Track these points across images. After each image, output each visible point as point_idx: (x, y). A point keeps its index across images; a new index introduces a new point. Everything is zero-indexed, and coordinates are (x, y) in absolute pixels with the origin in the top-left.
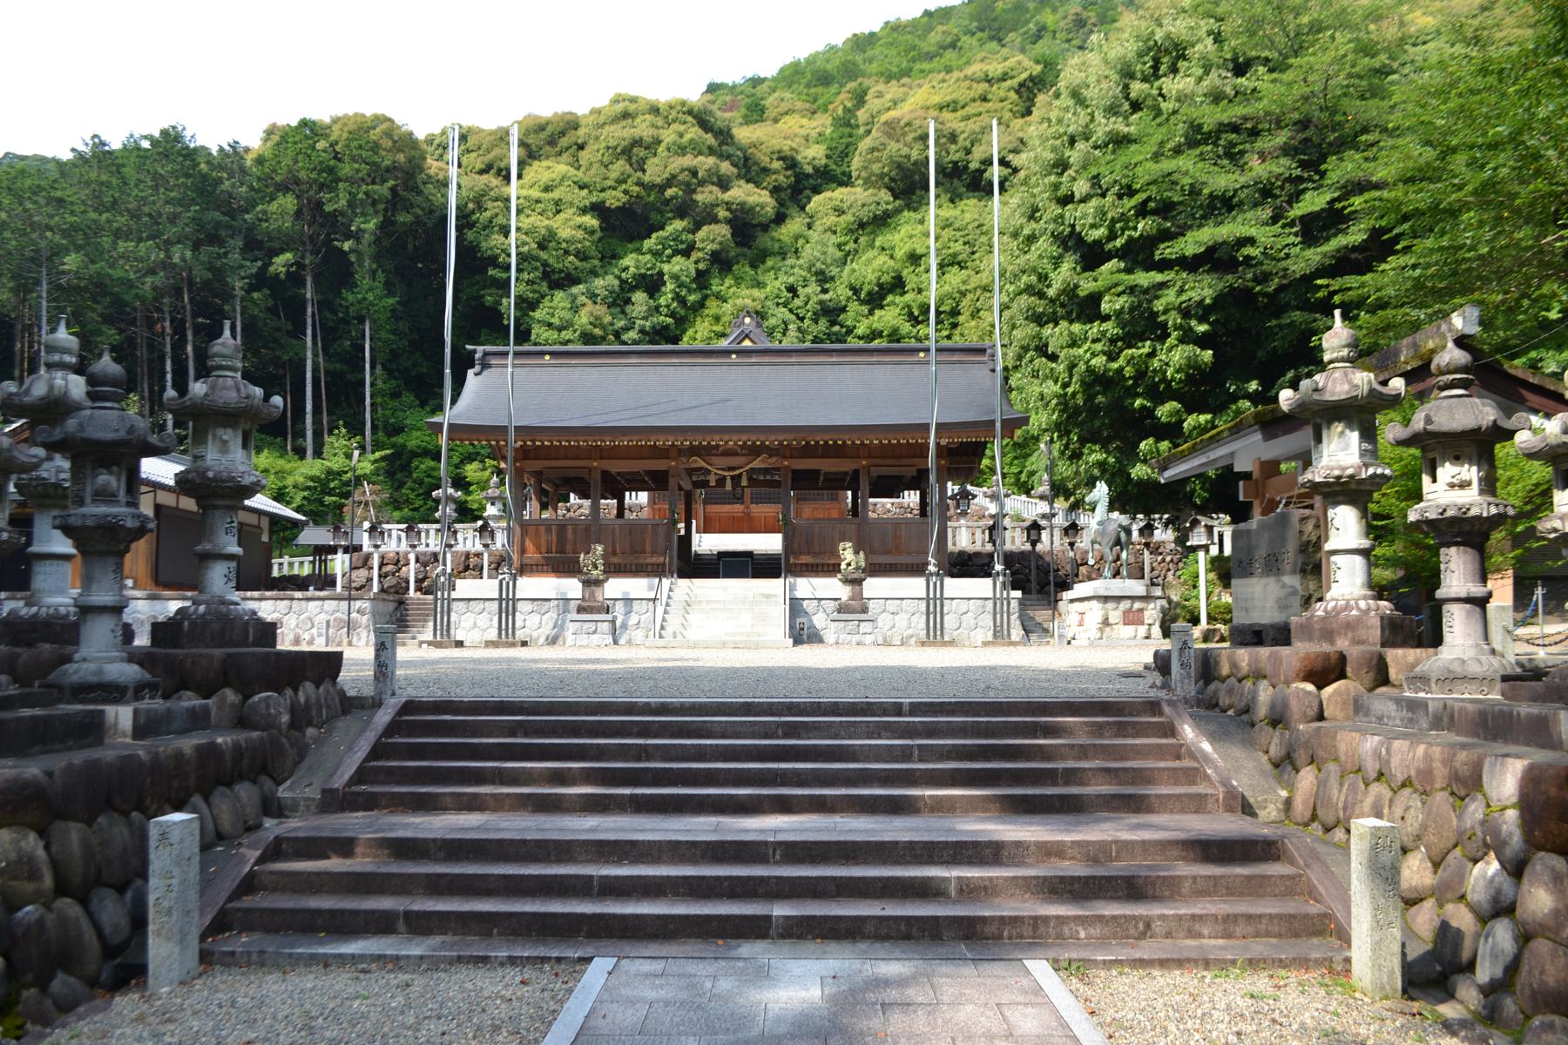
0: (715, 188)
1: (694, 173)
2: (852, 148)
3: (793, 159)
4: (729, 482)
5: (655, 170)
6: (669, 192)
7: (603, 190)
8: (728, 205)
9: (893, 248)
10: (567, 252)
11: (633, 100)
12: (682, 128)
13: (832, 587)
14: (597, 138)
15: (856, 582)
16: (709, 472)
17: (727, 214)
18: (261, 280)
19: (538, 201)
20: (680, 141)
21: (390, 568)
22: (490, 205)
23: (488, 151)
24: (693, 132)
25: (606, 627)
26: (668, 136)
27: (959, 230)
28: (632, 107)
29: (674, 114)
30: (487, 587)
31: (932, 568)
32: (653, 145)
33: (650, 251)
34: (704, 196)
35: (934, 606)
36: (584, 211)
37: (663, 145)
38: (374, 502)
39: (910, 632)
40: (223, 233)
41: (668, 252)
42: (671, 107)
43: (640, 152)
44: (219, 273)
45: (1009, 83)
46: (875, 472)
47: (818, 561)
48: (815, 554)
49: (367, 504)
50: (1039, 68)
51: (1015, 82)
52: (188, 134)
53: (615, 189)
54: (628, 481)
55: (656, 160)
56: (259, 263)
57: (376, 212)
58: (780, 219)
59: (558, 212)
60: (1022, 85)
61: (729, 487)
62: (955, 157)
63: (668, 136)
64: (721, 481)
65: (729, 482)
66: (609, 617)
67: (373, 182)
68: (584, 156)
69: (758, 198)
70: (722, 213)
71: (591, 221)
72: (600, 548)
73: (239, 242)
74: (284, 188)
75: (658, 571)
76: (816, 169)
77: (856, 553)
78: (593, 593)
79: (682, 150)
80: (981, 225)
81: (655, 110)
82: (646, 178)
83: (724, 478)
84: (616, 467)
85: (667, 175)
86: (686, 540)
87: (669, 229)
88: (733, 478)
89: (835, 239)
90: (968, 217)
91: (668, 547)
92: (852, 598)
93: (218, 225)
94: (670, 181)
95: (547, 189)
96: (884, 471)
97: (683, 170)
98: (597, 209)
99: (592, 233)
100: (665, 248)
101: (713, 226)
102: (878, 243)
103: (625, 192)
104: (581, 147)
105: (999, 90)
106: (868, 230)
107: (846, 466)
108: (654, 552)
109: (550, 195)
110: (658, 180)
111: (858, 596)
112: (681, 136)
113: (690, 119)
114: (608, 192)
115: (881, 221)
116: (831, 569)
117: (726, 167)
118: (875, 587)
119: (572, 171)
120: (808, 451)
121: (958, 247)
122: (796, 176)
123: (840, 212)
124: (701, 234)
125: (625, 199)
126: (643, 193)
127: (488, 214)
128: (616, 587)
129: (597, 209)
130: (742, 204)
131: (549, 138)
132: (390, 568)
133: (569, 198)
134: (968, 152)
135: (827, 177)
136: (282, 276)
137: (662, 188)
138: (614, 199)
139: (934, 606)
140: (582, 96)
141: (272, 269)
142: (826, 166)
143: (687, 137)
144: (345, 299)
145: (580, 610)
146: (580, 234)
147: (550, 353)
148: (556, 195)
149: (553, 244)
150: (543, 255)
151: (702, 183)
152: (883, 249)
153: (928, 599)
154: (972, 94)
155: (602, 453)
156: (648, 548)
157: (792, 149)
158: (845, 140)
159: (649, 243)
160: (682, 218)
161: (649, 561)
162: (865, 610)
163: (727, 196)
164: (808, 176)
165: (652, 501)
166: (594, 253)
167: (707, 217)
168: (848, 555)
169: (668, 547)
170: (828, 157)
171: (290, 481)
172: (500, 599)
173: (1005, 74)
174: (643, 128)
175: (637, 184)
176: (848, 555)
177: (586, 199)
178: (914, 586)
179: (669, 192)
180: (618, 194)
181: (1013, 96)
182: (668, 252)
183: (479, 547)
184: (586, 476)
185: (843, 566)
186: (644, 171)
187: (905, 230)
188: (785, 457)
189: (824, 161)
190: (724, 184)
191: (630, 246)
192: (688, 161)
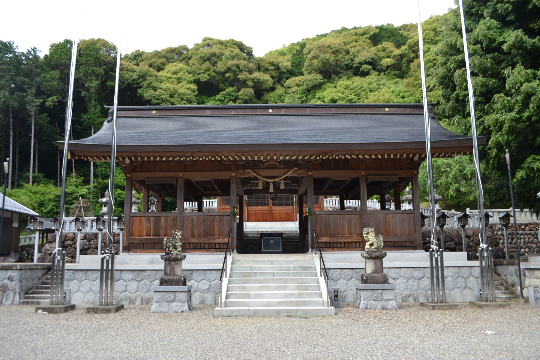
0: (247, 73)
1: (238, 67)
2: (302, 63)
3: (278, 66)
4: (271, 186)
5: (221, 66)
6: (227, 75)
7: (199, 74)
8: (252, 80)
9: (324, 98)
10: (182, 99)
11: (211, 39)
12: (232, 49)
13: (354, 259)
14: (196, 54)
15: (377, 257)
16: (258, 179)
17: (252, 84)
18: (42, 108)
19: (170, 78)
20: (231, 54)
21: (69, 242)
22: (149, 78)
23: (150, 59)
24: (237, 51)
25: (183, 296)
26: (227, 53)
27: (352, 89)
28: (211, 42)
29: (229, 44)
30: (91, 262)
31: (433, 247)
32: (219, 57)
33: (219, 100)
34: (241, 77)
35: (437, 272)
36: (191, 83)
37: (225, 56)
38: (84, 207)
39: (408, 292)
40: (25, 87)
41: (227, 100)
42: (228, 42)
43: (214, 59)
44: (23, 105)
45: (366, 36)
46: (371, 179)
47: (334, 240)
48: (332, 235)
49: (81, 208)
50: (378, 30)
51: (368, 36)
52: (15, 46)
53: (204, 74)
54: (205, 189)
55: (221, 62)
56: (42, 100)
57: (98, 80)
58: (273, 89)
59: (179, 83)
60: (371, 37)
61: (271, 190)
62: (346, 63)
63: (227, 53)
64: (266, 185)
65: (271, 186)
66: (185, 288)
67: (96, 66)
68: (191, 61)
69: (265, 77)
70: (250, 83)
71: (194, 87)
72: (179, 234)
73: (34, 91)
74: (54, 68)
75: (225, 248)
76: (288, 71)
77: (377, 235)
78: (173, 269)
79: (233, 58)
80: (362, 88)
81: (221, 43)
82: (217, 70)
83: (268, 183)
84: (196, 177)
85: (226, 68)
86: (240, 226)
87: (227, 90)
88: (274, 183)
89: (298, 96)
90: (356, 85)
91: (230, 232)
92: (375, 272)
93: (23, 83)
94: (229, 70)
95: (174, 73)
96: (377, 179)
97: (233, 65)
98: (197, 82)
99: (194, 92)
100: (225, 99)
101: (246, 89)
102: (316, 96)
103: (209, 75)
104: (190, 58)
105: (363, 38)
106: (311, 91)
107: (346, 175)
108: (220, 235)
109: (176, 76)
110: (222, 70)
111: (379, 269)
112: (232, 52)
113: (236, 47)
114: (201, 75)
115: (318, 87)
116: (359, 245)
117: (251, 65)
118: (394, 259)
119: (185, 67)
120: (325, 165)
121: (352, 96)
122: (280, 73)
123: (298, 85)
124: (241, 92)
125: (208, 78)
126: (216, 76)
127: (148, 82)
128: (194, 261)
129: (197, 82)
130: (258, 79)
131: (177, 54)
132: (69, 242)
133: (184, 77)
134: (352, 61)
135: (291, 73)
136: (52, 107)
137: (224, 73)
138: (204, 78)
139: (437, 272)
140: (190, 40)
141: (47, 103)
142: (292, 69)
143: (235, 53)
144: (83, 118)
145: (163, 282)
146: (188, 92)
147: (156, 109)
148: (178, 76)
149: (176, 95)
150: (172, 100)
151: (241, 71)
152: (319, 98)
153: (432, 267)
154: (352, 39)
155: (184, 166)
156: (216, 232)
157: (277, 62)
158: (299, 60)
159: (218, 97)
160: (233, 87)
161: (217, 241)
162: (385, 281)
163: (252, 76)
164: (284, 73)
165: (219, 204)
166: (194, 99)
167: (244, 84)
168: (371, 237)
169: (230, 232)
170: (292, 66)
171: (47, 197)
172: (102, 270)
173: (364, 32)
174: (215, 49)
175: (214, 72)
176: (371, 237)
177: (191, 77)
178: (419, 258)
179: (227, 75)
180: (206, 76)
181: (368, 41)
182: (227, 100)
183: (95, 230)
184: (174, 183)
185: (367, 246)
186: (217, 67)
187: (329, 90)
188: (309, 170)
189: (290, 67)
190: (251, 72)
191: (210, 98)
192: (235, 62)
